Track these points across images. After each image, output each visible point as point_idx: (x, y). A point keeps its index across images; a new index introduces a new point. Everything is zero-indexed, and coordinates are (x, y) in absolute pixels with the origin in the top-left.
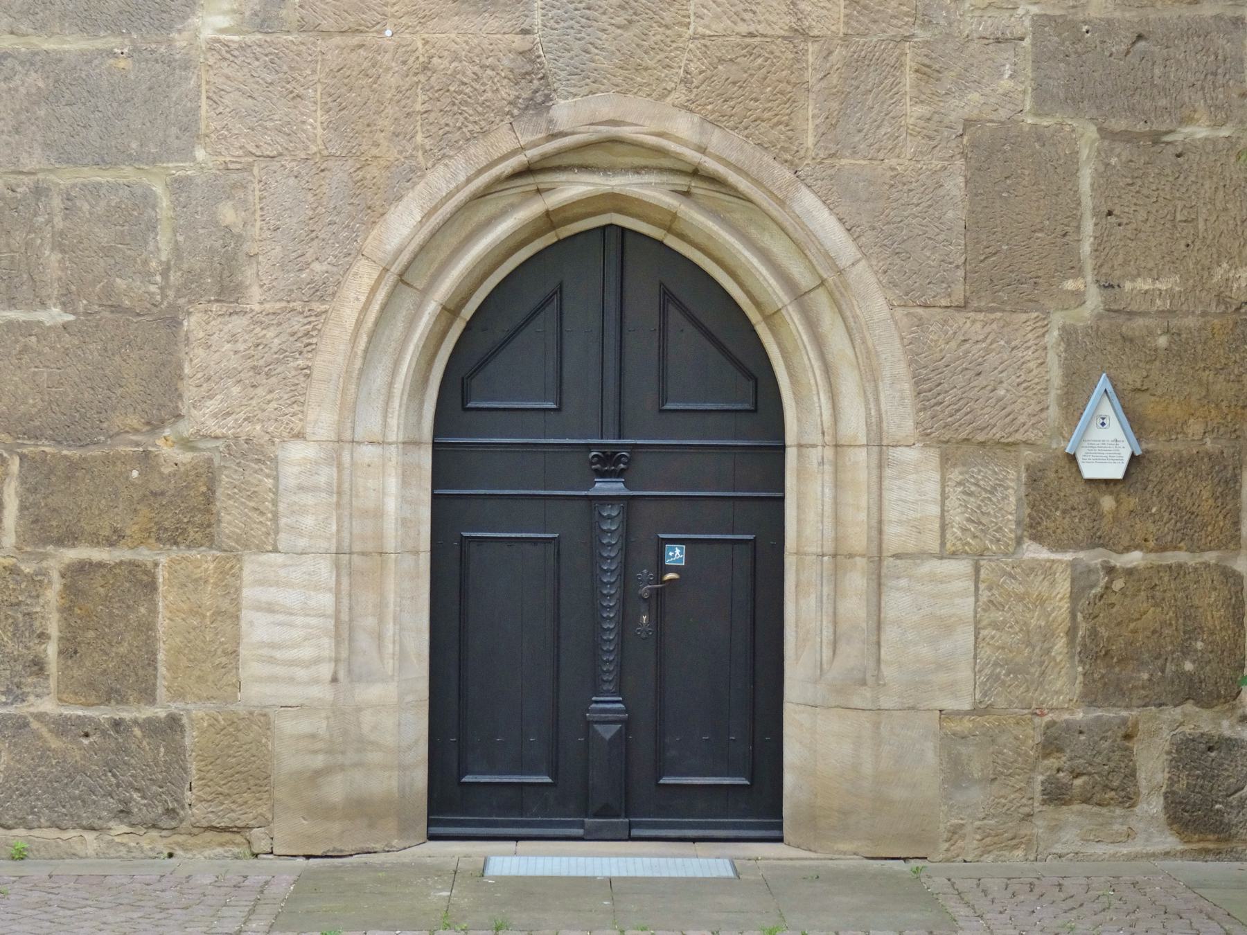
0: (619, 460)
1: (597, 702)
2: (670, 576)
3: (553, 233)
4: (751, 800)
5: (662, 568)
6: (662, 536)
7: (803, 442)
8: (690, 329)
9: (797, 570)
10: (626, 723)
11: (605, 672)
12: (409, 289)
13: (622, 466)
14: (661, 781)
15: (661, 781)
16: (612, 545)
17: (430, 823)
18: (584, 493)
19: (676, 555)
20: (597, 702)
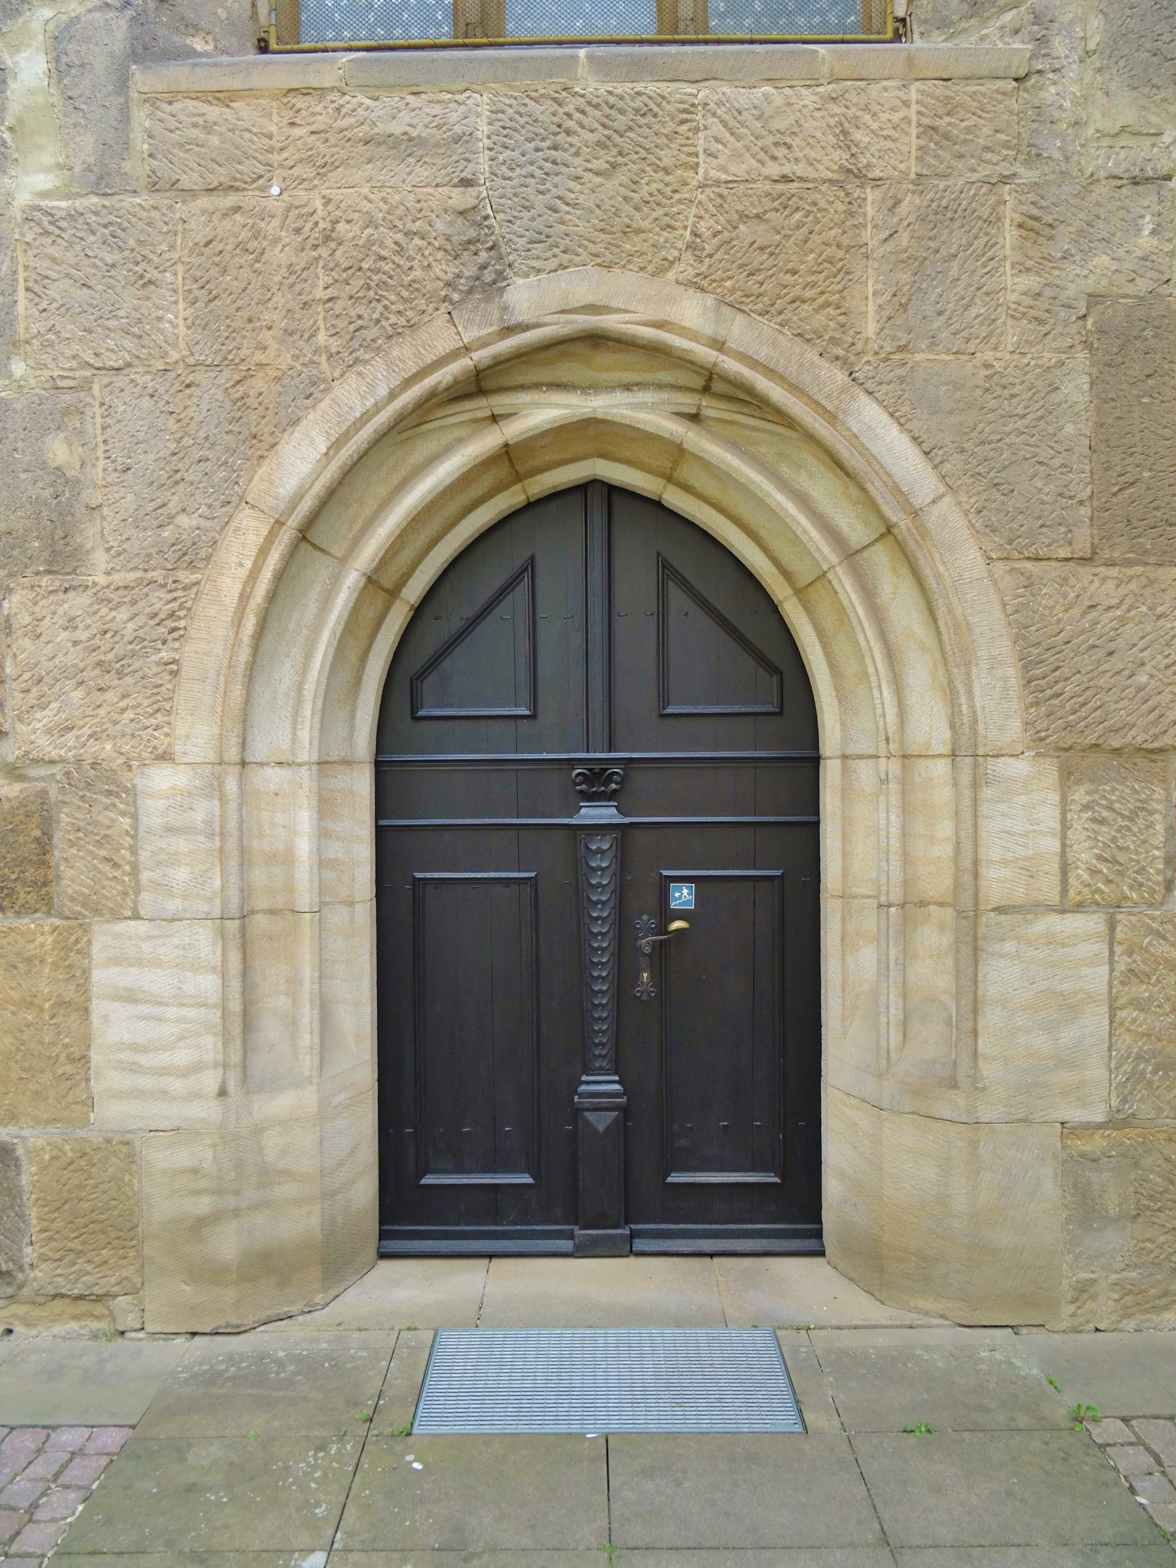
0: (609, 780)
1: (588, 1083)
2: (677, 925)
6: (666, 873)
7: (848, 752)
9: (843, 919)
10: (625, 1110)
11: (597, 1045)
12: (323, 557)
13: (613, 786)
14: (670, 1180)
15: (670, 1180)
16: (603, 886)
17: (383, 1235)
19: (683, 896)
20: (588, 1083)
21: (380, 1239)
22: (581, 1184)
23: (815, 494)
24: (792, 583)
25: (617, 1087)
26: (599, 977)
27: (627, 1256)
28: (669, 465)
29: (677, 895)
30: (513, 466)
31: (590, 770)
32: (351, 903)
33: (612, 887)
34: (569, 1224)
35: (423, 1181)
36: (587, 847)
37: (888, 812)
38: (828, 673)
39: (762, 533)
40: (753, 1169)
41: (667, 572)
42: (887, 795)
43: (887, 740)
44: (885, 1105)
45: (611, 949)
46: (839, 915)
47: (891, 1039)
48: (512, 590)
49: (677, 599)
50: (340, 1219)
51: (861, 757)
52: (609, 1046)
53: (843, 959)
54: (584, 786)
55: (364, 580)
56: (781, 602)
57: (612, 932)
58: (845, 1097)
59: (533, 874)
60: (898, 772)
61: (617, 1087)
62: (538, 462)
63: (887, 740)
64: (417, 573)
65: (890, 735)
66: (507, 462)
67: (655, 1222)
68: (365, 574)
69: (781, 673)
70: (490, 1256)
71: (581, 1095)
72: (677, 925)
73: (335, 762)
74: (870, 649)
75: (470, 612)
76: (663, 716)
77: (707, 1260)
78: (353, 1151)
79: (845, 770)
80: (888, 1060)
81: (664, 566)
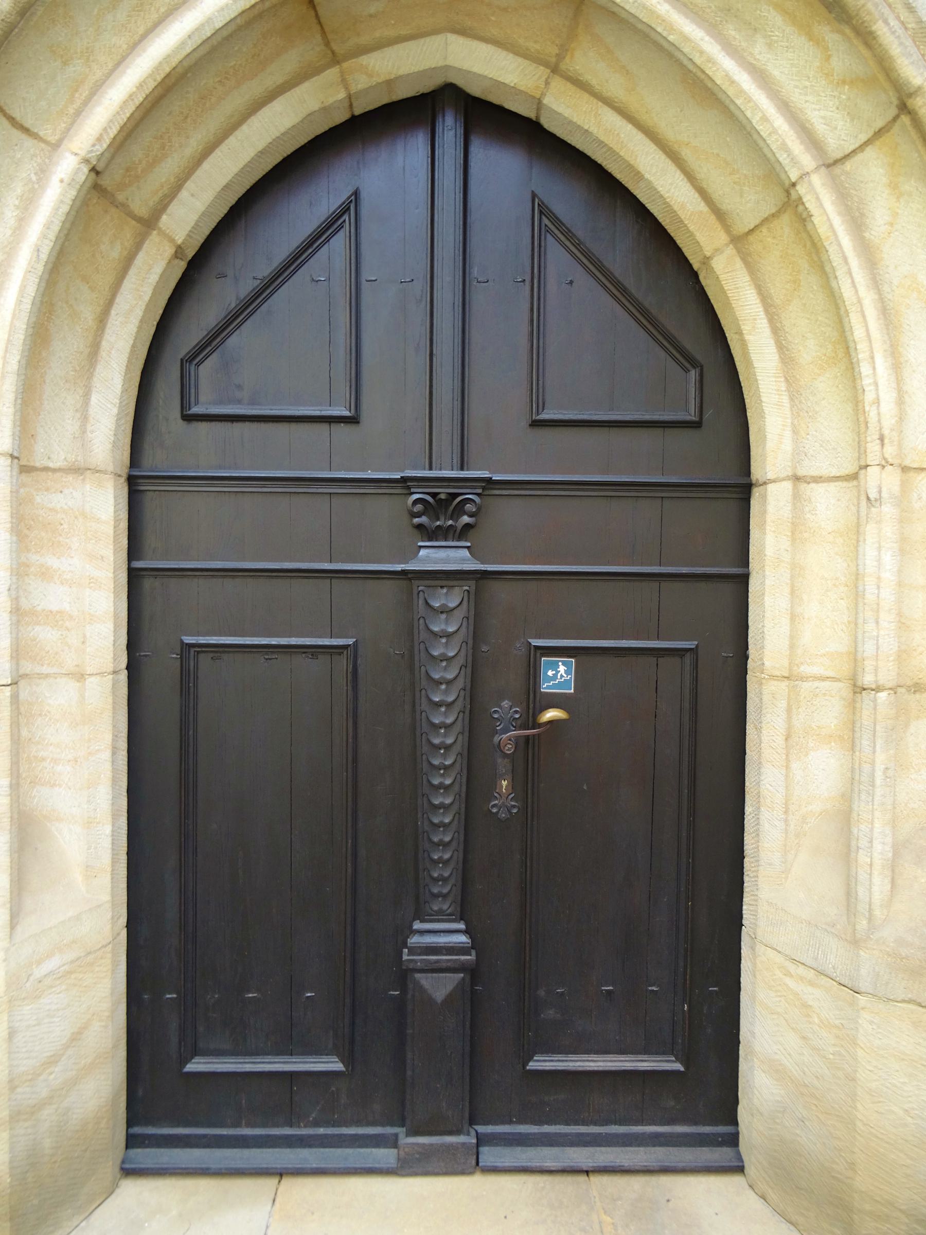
0: (459, 510)
1: (422, 932)
2: (551, 714)
3: (332, 73)
4: (690, 1096)
5: (535, 701)
6: (536, 642)
7: (801, 473)
8: (584, 282)
9: (789, 710)
10: (473, 973)
11: (436, 880)
12: (29, 142)
13: (466, 519)
14: (532, 1065)
15: (532, 1065)
16: (449, 659)
17: (132, 1141)
18: (399, 567)
19: (559, 675)
20: (422, 932)
21: (127, 1147)
22: (409, 1073)
23: (776, 73)
24: (727, 228)
25: (463, 939)
26: (441, 786)
27: (471, 1173)
28: (555, 50)
29: (550, 673)
30: (327, 44)
31: (434, 495)
32: (80, 677)
33: (461, 660)
34: (392, 1125)
35: (190, 1067)
36: (427, 603)
37: (879, 549)
38: (776, 357)
39: (686, 154)
40: (646, 1050)
41: (545, 221)
42: (879, 522)
43: (882, 439)
44: (864, 986)
45: (457, 748)
46: (783, 704)
47: (875, 889)
48: (328, 240)
49: (557, 257)
50: (47, 1143)
51: (817, 480)
52: (452, 865)
53: (787, 767)
54: (424, 520)
55: (86, 170)
56: (706, 260)
57: (459, 723)
58: (788, 964)
59: (351, 641)
60: (896, 489)
61: (463, 939)
62: (364, 39)
63: (882, 439)
64: (184, 194)
65: (886, 432)
66: (318, 37)
67: (510, 1122)
68: (86, 161)
69: (702, 367)
70: (281, 1174)
71: (412, 951)
72: (551, 714)
73: (59, 470)
74: (859, 301)
75: (265, 270)
76: (536, 424)
77: (582, 1178)
78: (76, 1037)
79: (796, 496)
80: (870, 920)
81: (541, 213)
